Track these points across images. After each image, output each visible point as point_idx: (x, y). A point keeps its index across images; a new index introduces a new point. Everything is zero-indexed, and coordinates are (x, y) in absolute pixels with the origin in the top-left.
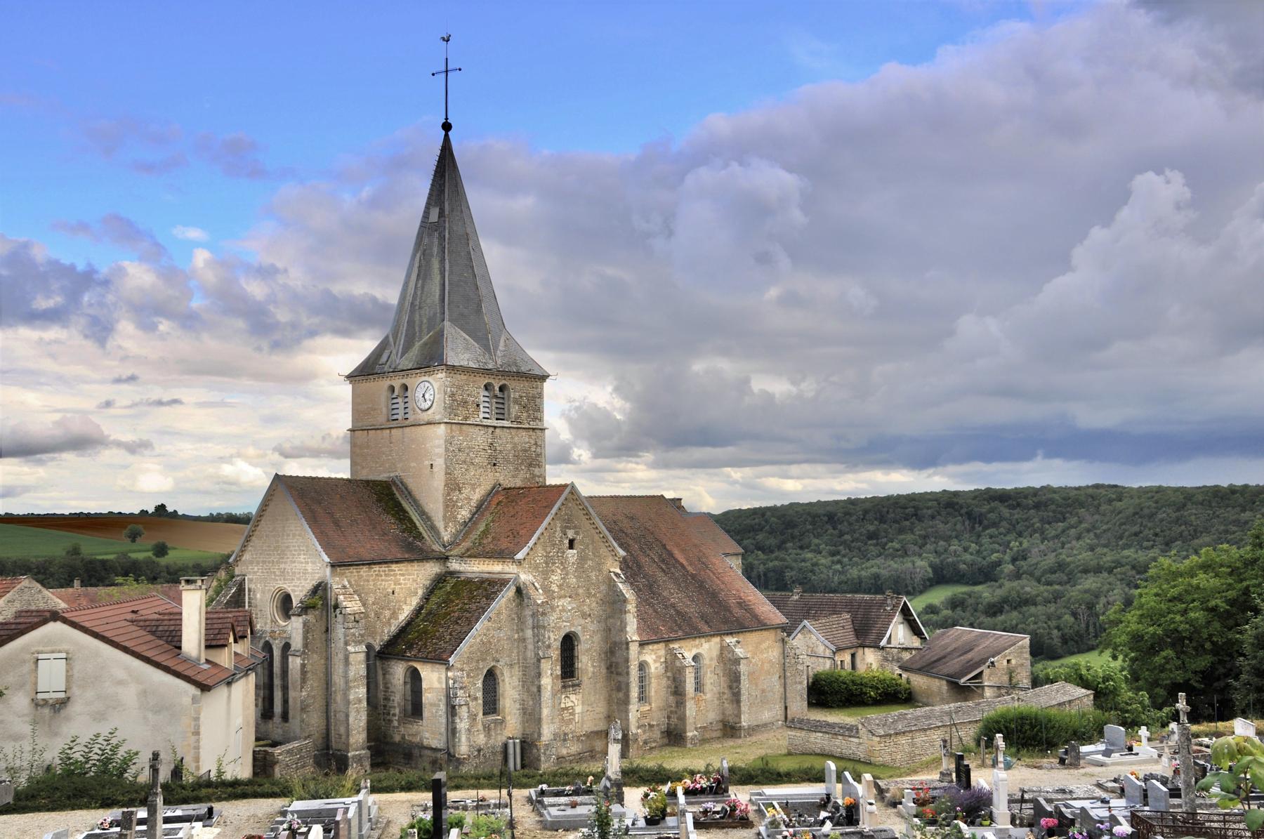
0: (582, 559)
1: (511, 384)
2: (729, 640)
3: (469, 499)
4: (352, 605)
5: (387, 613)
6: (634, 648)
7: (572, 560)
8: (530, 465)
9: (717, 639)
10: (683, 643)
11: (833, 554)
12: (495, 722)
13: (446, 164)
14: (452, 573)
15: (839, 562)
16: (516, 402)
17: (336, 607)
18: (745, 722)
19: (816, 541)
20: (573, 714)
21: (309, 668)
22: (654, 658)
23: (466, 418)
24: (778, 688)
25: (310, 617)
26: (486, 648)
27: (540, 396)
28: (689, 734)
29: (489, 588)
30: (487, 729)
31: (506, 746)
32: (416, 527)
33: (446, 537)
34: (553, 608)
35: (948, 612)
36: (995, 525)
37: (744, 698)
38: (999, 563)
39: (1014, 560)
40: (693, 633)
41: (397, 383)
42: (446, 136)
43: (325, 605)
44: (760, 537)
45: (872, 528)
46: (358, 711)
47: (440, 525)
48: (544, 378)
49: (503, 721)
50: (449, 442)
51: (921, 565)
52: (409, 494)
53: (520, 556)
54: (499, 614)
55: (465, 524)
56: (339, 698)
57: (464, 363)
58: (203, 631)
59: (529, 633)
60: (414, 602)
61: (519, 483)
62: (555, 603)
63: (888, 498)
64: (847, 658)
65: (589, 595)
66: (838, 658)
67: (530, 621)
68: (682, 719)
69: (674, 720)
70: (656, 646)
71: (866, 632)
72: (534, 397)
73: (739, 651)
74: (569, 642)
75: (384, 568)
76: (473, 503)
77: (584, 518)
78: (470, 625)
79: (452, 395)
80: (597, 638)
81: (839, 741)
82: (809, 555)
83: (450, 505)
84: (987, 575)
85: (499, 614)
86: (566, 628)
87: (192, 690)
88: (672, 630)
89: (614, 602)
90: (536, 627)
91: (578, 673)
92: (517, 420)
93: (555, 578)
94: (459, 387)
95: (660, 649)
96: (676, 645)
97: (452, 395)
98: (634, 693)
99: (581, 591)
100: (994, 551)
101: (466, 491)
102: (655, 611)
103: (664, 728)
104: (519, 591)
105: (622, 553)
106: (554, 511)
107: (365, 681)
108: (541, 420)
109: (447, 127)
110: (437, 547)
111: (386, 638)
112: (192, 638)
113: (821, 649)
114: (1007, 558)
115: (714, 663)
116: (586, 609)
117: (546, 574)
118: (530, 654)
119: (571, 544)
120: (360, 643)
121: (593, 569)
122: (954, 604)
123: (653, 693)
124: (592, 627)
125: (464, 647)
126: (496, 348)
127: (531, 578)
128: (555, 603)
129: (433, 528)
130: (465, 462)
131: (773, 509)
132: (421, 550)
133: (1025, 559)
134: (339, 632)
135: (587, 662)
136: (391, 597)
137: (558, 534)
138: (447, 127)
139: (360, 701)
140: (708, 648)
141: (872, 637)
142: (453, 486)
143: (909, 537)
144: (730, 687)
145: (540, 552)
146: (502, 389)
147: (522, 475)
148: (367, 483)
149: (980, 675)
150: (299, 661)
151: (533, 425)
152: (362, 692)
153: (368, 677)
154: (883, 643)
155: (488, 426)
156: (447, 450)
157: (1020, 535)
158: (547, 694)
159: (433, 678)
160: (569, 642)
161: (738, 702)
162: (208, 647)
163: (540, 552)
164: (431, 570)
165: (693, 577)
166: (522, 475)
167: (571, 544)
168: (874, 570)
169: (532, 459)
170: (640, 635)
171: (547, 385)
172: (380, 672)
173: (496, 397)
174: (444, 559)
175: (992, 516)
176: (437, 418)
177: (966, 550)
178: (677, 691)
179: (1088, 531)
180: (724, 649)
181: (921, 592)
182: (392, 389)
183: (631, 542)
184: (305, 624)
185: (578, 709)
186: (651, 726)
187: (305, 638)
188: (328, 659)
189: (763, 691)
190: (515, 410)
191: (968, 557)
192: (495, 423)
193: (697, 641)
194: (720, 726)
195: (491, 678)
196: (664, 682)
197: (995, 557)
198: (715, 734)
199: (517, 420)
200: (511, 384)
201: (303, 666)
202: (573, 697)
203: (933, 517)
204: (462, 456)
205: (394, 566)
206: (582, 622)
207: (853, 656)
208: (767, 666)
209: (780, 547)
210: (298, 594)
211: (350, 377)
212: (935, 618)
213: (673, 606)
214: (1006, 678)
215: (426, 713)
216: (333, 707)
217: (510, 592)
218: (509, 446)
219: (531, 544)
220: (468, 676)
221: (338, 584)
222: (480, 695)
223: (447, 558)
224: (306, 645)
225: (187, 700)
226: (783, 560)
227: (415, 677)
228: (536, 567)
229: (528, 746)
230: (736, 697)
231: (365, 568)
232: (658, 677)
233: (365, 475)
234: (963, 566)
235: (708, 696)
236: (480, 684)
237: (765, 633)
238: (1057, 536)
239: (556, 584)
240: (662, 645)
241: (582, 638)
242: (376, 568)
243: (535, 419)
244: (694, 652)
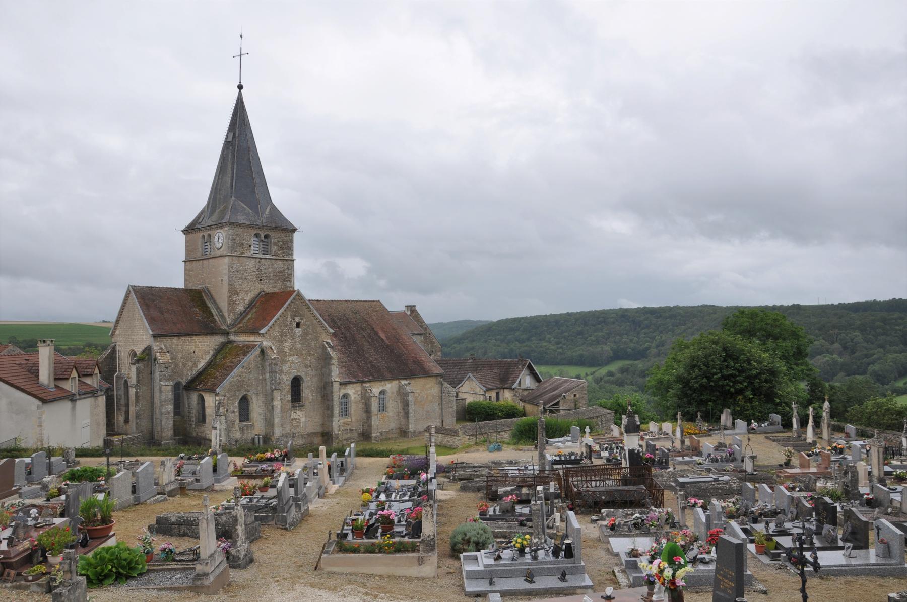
0: (305, 334)
1: (272, 234)
2: (403, 382)
3: (244, 300)
4: (162, 359)
5: (190, 364)
6: (336, 386)
7: (298, 334)
8: (284, 280)
9: (397, 382)
10: (372, 384)
11: (558, 343)
12: (247, 426)
13: (240, 111)
14: (231, 342)
15: (561, 348)
16: (275, 244)
17: (155, 360)
18: (412, 428)
19: (549, 336)
20: (299, 422)
21: (140, 394)
22: (353, 391)
23: (242, 253)
24: (438, 410)
25: (140, 365)
26: (240, 384)
27: (292, 241)
28: (374, 435)
29: (246, 349)
30: (242, 430)
31: (253, 439)
32: (212, 315)
33: (229, 321)
34: (286, 362)
35: (619, 375)
36: (648, 327)
37: (411, 415)
38: (648, 349)
39: (657, 346)
40: (379, 376)
41: (206, 234)
42: (240, 92)
43: (149, 359)
44: (517, 334)
45: (579, 329)
46: (167, 418)
47: (226, 314)
48: (294, 230)
49: (252, 426)
50: (231, 267)
51: (607, 349)
52: (212, 298)
53: (263, 331)
54: (249, 364)
55: (241, 314)
56: (157, 411)
57: (242, 222)
58: (52, 370)
59: (268, 375)
60: (208, 358)
61: (276, 290)
62: (287, 358)
63: (589, 312)
64: (493, 394)
66: (488, 395)
67: (268, 369)
68: (370, 426)
69: (366, 427)
70: (355, 385)
71: (505, 380)
72: (287, 242)
73: (408, 389)
74: (296, 383)
75: (188, 338)
76: (247, 302)
77: (306, 310)
78: (232, 369)
79: (233, 240)
80: (315, 380)
81: (449, 439)
82: (545, 344)
83: (232, 303)
84: (641, 355)
85: (249, 364)
86: (295, 373)
87: (37, 402)
88: (366, 376)
89: (326, 359)
90: (272, 372)
91: (303, 399)
92: (275, 254)
93: (287, 344)
94: (237, 235)
95: (358, 387)
96: (368, 385)
97: (233, 240)
98: (336, 411)
100: (647, 342)
101: (241, 296)
102: (358, 365)
103: (360, 431)
104: (262, 351)
105: (331, 331)
106: (285, 306)
107: (172, 402)
108: (292, 255)
109: (240, 87)
110: (224, 327)
111: (190, 378)
112: (45, 375)
113: (478, 390)
114: (653, 345)
115: (395, 395)
118: (268, 388)
119: (298, 325)
120: (169, 380)
122: (623, 371)
123: (353, 412)
124: (312, 373)
125: (226, 383)
126: (263, 212)
127: (270, 344)
128: (287, 358)
129: (222, 316)
131: (526, 318)
132: (213, 328)
133: (663, 345)
134: (157, 374)
135: (308, 392)
136: (193, 355)
137: (289, 319)
138: (240, 87)
139: (169, 413)
140: (390, 387)
141: (509, 382)
142: (233, 292)
143: (600, 334)
144: (404, 409)
145: (277, 328)
146: (266, 236)
147: (278, 286)
148: (191, 291)
149: (557, 404)
150: (134, 390)
151: (286, 257)
152: (170, 408)
153: (175, 400)
154: (515, 385)
156: (229, 271)
157: (661, 332)
158: (277, 411)
159: (210, 401)
160: (296, 383)
161: (408, 417)
162: (56, 379)
163: (277, 328)
164: (219, 339)
166: (278, 286)
167: (298, 325)
168: (580, 352)
169: (287, 276)
171: (296, 235)
172: (186, 398)
173: (262, 241)
174: (227, 333)
175: (646, 322)
176: (225, 253)
177: (631, 341)
178: (368, 411)
179: (698, 330)
180: (400, 387)
181: (606, 365)
182: (203, 236)
183: (352, 326)
184: (137, 369)
185: (303, 420)
186: (351, 430)
187: (138, 377)
188: (152, 389)
189: (428, 412)
190: (274, 249)
191: (632, 345)
192: (261, 256)
193: (383, 383)
194: (398, 431)
195: (244, 402)
196: (361, 405)
197: (647, 345)
198: (394, 436)
199: (275, 254)
200: (272, 234)
201: (137, 393)
202: (299, 413)
203: (613, 323)
204: (239, 275)
205: (194, 337)
206: (305, 370)
207: (498, 393)
208: (430, 398)
209: (528, 339)
210: (139, 350)
211: (184, 231)
212: (612, 378)
213: (370, 362)
214: (573, 405)
215: (207, 421)
216: (155, 416)
217: (257, 352)
218: (270, 270)
219: (270, 324)
220: (229, 399)
221: (156, 346)
222: (237, 410)
223: (228, 333)
224: (138, 381)
225: (34, 408)
226: (530, 347)
227: (202, 400)
228: (274, 338)
229: (267, 439)
230: (407, 414)
231: (176, 338)
232: (356, 402)
233: (190, 287)
234: (629, 350)
235: (390, 414)
236: (237, 404)
237: (429, 379)
238: (681, 333)
239: (284, 348)
240: (359, 385)
241: (305, 379)
242: (183, 338)
244: (381, 389)
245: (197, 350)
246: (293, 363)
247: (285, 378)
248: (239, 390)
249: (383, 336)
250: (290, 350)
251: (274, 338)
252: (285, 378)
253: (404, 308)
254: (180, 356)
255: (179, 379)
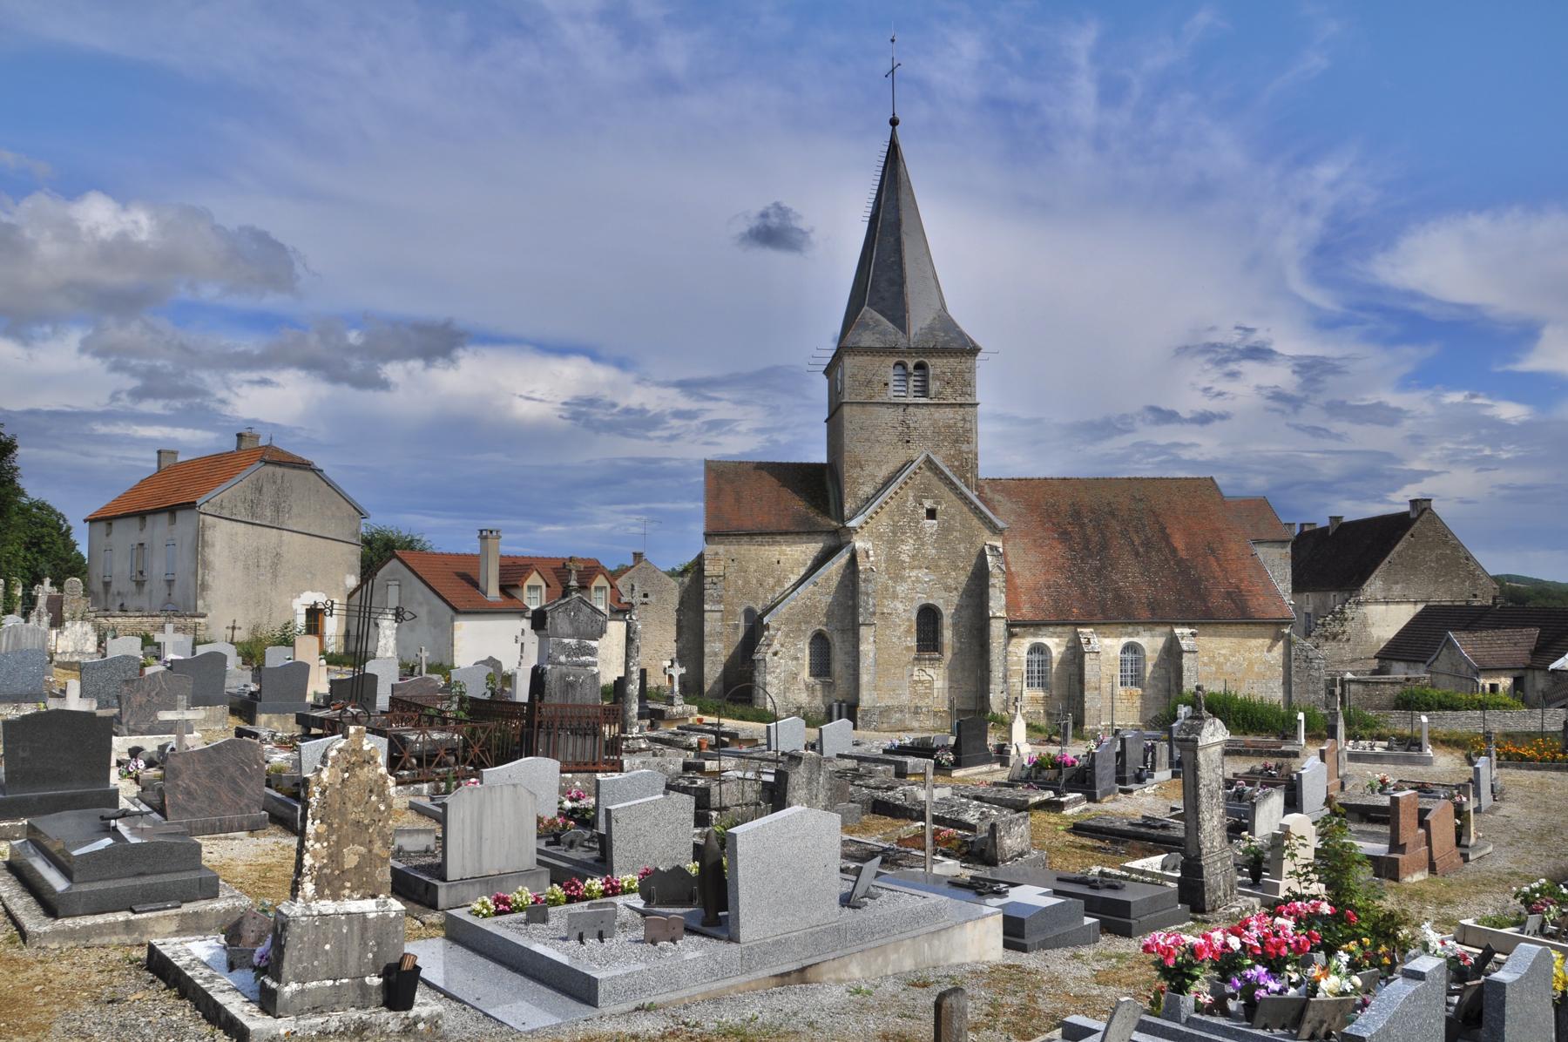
0: (945, 531)
5: (771, 581)
8: (957, 441)
13: (893, 154)
20: (931, 688)
34: (903, 579)
48: (974, 351)
62: (906, 573)
65: (956, 568)
72: (962, 372)
85: (828, 579)
87: (451, 612)
93: (907, 548)
99: (942, 563)
101: (869, 469)
109: (894, 122)
116: (950, 582)
117: (893, 542)
119: (931, 514)
121: (961, 541)
127: (869, 545)
128: (906, 573)
130: (868, 440)
137: (911, 503)
138: (894, 122)
145: (884, 518)
146: (920, 366)
155: (898, 404)
163: (884, 518)
165: (1180, 562)
170: (1007, 611)
190: (934, 386)
202: (931, 671)
206: (946, 595)
228: (880, 536)
243: (963, 394)
245: (783, 559)
246: (918, 580)
247: (900, 607)
248: (807, 623)
249: (1179, 542)
250: (913, 557)
251: (880, 536)
252: (900, 607)
253: (1407, 508)
254: (752, 567)
255: (752, 604)
